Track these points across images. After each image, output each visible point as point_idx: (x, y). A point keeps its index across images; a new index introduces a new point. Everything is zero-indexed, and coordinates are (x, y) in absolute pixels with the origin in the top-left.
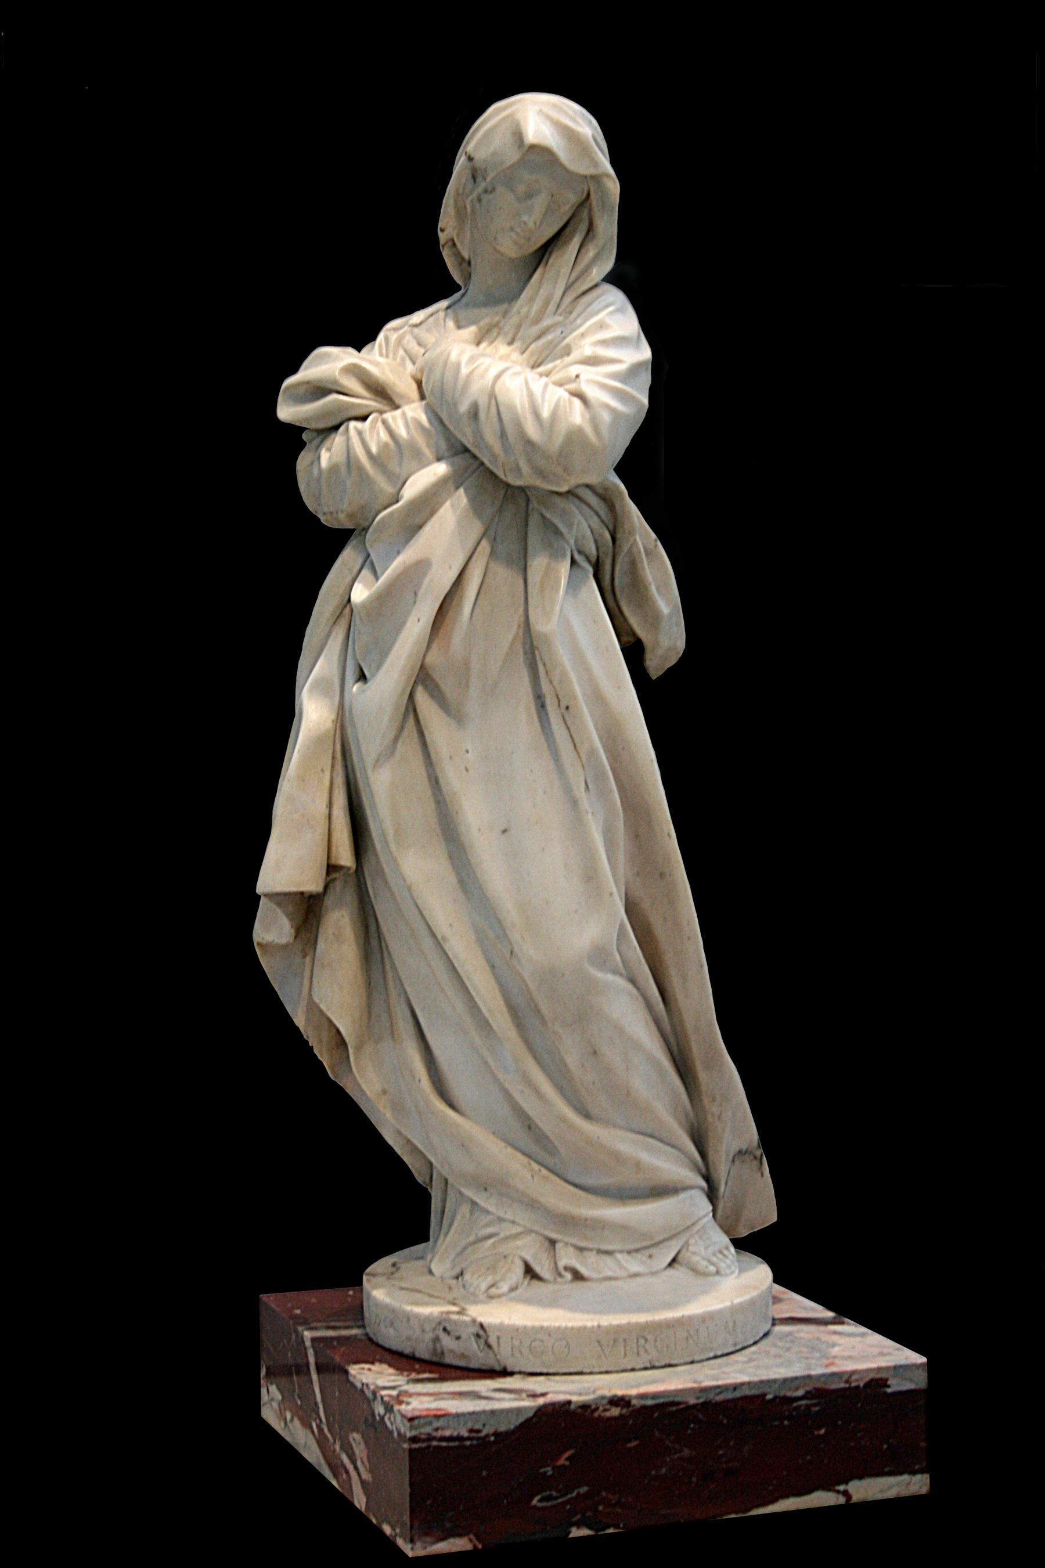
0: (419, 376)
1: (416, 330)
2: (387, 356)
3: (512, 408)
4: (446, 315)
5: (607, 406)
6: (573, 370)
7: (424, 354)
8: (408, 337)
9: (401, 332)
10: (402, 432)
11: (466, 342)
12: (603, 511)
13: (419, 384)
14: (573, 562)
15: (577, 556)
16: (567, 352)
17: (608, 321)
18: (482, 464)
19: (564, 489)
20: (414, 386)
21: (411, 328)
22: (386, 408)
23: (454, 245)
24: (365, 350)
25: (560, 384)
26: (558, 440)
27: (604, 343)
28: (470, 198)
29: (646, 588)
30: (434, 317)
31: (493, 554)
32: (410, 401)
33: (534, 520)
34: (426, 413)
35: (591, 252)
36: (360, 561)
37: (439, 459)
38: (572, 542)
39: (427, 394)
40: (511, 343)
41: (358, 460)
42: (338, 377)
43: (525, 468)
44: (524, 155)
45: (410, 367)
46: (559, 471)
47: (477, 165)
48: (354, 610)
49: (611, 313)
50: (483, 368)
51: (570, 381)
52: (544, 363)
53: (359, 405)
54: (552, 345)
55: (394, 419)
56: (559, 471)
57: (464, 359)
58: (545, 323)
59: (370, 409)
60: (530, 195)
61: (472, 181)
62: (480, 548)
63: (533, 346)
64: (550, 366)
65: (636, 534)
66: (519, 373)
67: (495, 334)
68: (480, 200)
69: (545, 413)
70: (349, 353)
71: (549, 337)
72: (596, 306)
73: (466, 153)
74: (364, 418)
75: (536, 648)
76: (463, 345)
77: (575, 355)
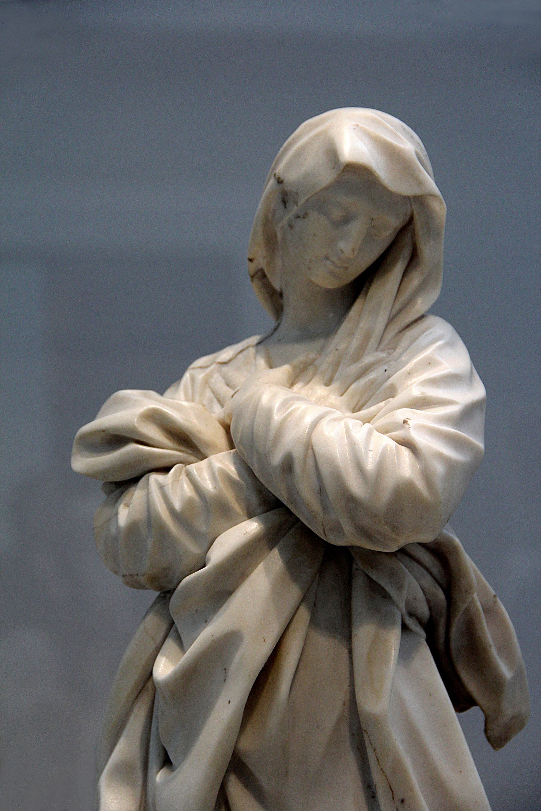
0: (227, 421)
1: (225, 369)
2: (193, 401)
3: (331, 461)
4: (257, 352)
5: (440, 456)
6: (401, 414)
7: (232, 397)
8: (216, 376)
9: (208, 370)
10: (208, 485)
11: (277, 384)
12: (436, 569)
13: (227, 428)
14: (405, 628)
15: (409, 622)
16: (392, 392)
17: (438, 357)
18: (298, 520)
19: (394, 548)
20: (221, 432)
21: (218, 365)
22: (191, 458)
23: (264, 276)
24: (169, 392)
25: (385, 431)
26: (385, 496)
27: (434, 382)
28: (280, 225)
29: (486, 651)
30: (244, 353)
31: (314, 622)
32: (216, 450)
33: (359, 582)
34: (235, 464)
35: (415, 280)
36: (164, 628)
37: (250, 515)
38: (402, 605)
39: (236, 442)
40: (328, 383)
41: (159, 518)
42: (136, 425)
43: (347, 528)
44: (339, 176)
45: (218, 411)
46: (387, 530)
47: (286, 189)
48: (158, 689)
49: (440, 348)
50: (299, 412)
51: (396, 427)
52: (365, 407)
53: (162, 456)
54: (374, 386)
55: (198, 470)
56: (387, 530)
57: (277, 404)
58: (368, 359)
59: (174, 460)
60: (346, 220)
61: (282, 205)
62: (298, 616)
63: (353, 386)
64: (373, 408)
65: (473, 593)
66: (341, 419)
67: (311, 374)
68: (291, 227)
69: (370, 465)
70: (150, 397)
71: (372, 376)
72: (422, 340)
73: (275, 175)
74: (166, 470)
75: (365, 731)
76: (277, 389)
77: (402, 396)
